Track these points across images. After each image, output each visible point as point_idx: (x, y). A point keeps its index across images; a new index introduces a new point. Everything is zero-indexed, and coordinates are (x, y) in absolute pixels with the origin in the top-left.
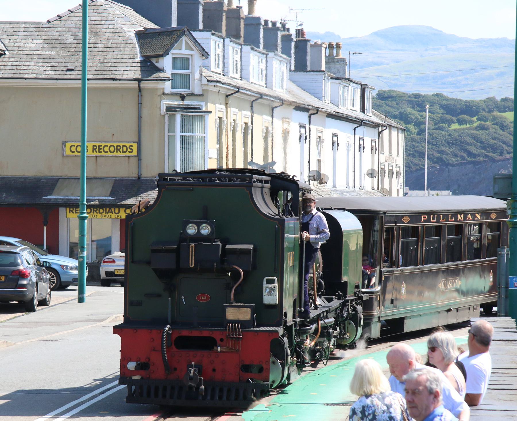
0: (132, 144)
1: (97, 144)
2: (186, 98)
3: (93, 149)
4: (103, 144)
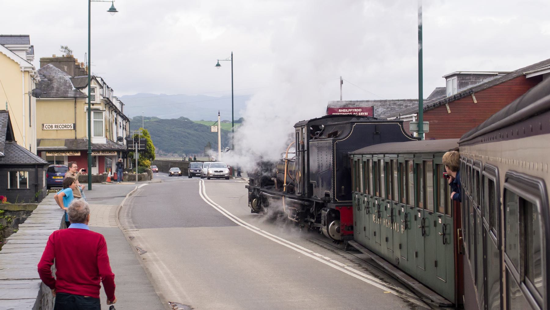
0: (71, 124)
1: (57, 125)
2: (94, 105)
3: (55, 127)
4: (59, 125)
